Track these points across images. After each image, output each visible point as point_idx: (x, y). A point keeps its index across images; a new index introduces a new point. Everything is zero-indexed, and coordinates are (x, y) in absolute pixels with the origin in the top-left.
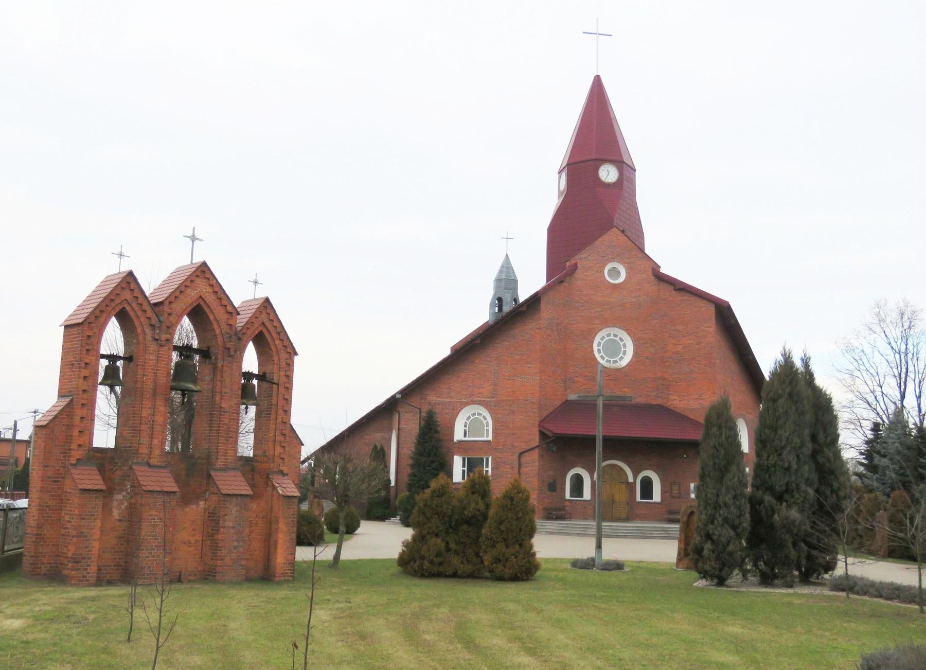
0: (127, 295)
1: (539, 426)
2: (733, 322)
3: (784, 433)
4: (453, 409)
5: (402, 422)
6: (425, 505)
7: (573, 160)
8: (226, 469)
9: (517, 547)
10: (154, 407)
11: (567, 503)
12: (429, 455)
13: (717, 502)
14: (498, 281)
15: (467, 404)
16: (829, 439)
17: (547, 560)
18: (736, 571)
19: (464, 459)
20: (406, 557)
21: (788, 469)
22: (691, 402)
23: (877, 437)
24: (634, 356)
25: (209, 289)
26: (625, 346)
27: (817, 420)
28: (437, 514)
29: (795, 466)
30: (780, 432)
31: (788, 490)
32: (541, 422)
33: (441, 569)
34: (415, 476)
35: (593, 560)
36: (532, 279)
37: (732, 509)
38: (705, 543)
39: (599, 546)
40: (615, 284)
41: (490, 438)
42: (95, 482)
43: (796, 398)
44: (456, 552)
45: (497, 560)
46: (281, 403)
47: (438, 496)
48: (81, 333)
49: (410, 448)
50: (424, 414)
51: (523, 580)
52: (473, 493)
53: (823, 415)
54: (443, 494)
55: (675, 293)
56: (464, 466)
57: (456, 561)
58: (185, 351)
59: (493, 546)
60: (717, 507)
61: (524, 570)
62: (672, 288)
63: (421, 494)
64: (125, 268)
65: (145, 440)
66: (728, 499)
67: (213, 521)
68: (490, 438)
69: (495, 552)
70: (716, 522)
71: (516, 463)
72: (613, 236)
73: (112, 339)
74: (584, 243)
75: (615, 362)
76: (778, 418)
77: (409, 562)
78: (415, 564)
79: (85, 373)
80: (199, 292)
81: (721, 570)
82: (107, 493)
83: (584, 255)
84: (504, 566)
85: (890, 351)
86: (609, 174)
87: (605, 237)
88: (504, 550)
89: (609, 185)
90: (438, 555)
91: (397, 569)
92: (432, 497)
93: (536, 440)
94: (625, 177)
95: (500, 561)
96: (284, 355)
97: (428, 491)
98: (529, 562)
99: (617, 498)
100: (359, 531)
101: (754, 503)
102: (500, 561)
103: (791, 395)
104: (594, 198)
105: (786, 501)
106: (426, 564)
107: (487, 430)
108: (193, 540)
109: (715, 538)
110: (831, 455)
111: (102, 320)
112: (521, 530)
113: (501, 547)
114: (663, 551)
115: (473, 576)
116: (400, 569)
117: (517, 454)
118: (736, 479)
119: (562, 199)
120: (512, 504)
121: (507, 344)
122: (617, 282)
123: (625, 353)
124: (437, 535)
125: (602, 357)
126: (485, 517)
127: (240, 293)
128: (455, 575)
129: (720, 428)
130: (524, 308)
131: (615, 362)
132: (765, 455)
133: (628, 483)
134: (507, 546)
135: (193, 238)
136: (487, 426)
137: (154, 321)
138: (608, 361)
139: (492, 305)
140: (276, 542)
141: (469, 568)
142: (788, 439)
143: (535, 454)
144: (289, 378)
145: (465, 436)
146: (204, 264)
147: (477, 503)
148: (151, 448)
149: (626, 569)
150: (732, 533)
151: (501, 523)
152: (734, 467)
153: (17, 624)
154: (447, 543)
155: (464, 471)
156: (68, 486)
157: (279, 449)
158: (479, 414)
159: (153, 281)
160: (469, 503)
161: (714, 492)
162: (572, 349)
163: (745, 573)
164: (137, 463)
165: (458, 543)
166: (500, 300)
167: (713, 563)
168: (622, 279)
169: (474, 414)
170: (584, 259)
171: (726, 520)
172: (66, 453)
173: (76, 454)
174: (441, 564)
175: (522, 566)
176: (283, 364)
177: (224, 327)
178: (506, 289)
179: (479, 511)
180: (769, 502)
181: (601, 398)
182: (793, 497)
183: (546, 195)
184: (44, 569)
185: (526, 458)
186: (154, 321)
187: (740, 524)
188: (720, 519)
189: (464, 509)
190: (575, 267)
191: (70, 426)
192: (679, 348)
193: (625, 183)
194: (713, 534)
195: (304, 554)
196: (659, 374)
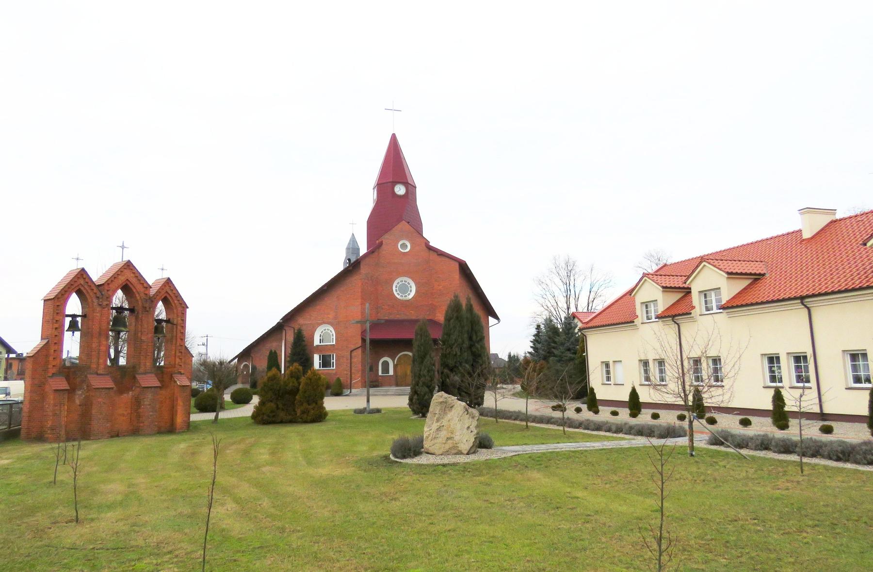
0: (82, 282)
3: (453, 337)
8: (145, 373)
10: (100, 342)
14: (348, 249)
15: (321, 324)
17: (332, 412)
21: (456, 355)
23: (538, 332)
25: (132, 275)
27: (472, 329)
29: (459, 353)
31: (455, 366)
36: (363, 250)
39: (368, 401)
42: (64, 385)
44: (283, 410)
45: (303, 412)
46: (179, 334)
48: (54, 304)
49: (289, 351)
57: (282, 415)
58: (120, 310)
59: (302, 404)
60: (420, 377)
61: (320, 416)
64: (80, 266)
65: (94, 360)
66: (425, 372)
67: (137, 402)
69: (302, 408)
72: (403, 225)
73: (74, 306)
74: (387, 230)
78: (262, 418)
79: (56, 326)
80: (127, 277)
82: (71, 391)
83: (386, 236)
85: (561, 284)
86: (400, 190)
89: (403, 196)
90: (272, 412)
91: (251, 421)
96: (180, 309)
103: (457, 318)
104: (394, 201)
108: (125, 413)
111: (66, 296)
113: (305, 405)
115: (292, 421)
126: (298, 390)
127: (152, 276)
129: (421, 336)
135: (123, 247)
137: (99, 294)
139: (345, 263)
140: (176, 411)
141: (289, 417)
144: (184, 321)
146: (129, 261)
148: (98, 364)
149: (383, 412)
150: (427, 389)
153: (6, 462)
156: (48, 388)
157: (178, 360)
159: (96, 274)
162: (378, 290)
164: (90, 374)
165: (284, 405)
166: (349, 260)
168: (408, 250)
170: (386, 239)
172: (46, 370)
173: (52, 370)
176: (180, 314)
177: (142, 295)
183: (365, 201)
184: (33, 435)
185: (354, 354)
186: (99, 294)
190: (381, 244)
191: (47, 356)
195: (197, 417)
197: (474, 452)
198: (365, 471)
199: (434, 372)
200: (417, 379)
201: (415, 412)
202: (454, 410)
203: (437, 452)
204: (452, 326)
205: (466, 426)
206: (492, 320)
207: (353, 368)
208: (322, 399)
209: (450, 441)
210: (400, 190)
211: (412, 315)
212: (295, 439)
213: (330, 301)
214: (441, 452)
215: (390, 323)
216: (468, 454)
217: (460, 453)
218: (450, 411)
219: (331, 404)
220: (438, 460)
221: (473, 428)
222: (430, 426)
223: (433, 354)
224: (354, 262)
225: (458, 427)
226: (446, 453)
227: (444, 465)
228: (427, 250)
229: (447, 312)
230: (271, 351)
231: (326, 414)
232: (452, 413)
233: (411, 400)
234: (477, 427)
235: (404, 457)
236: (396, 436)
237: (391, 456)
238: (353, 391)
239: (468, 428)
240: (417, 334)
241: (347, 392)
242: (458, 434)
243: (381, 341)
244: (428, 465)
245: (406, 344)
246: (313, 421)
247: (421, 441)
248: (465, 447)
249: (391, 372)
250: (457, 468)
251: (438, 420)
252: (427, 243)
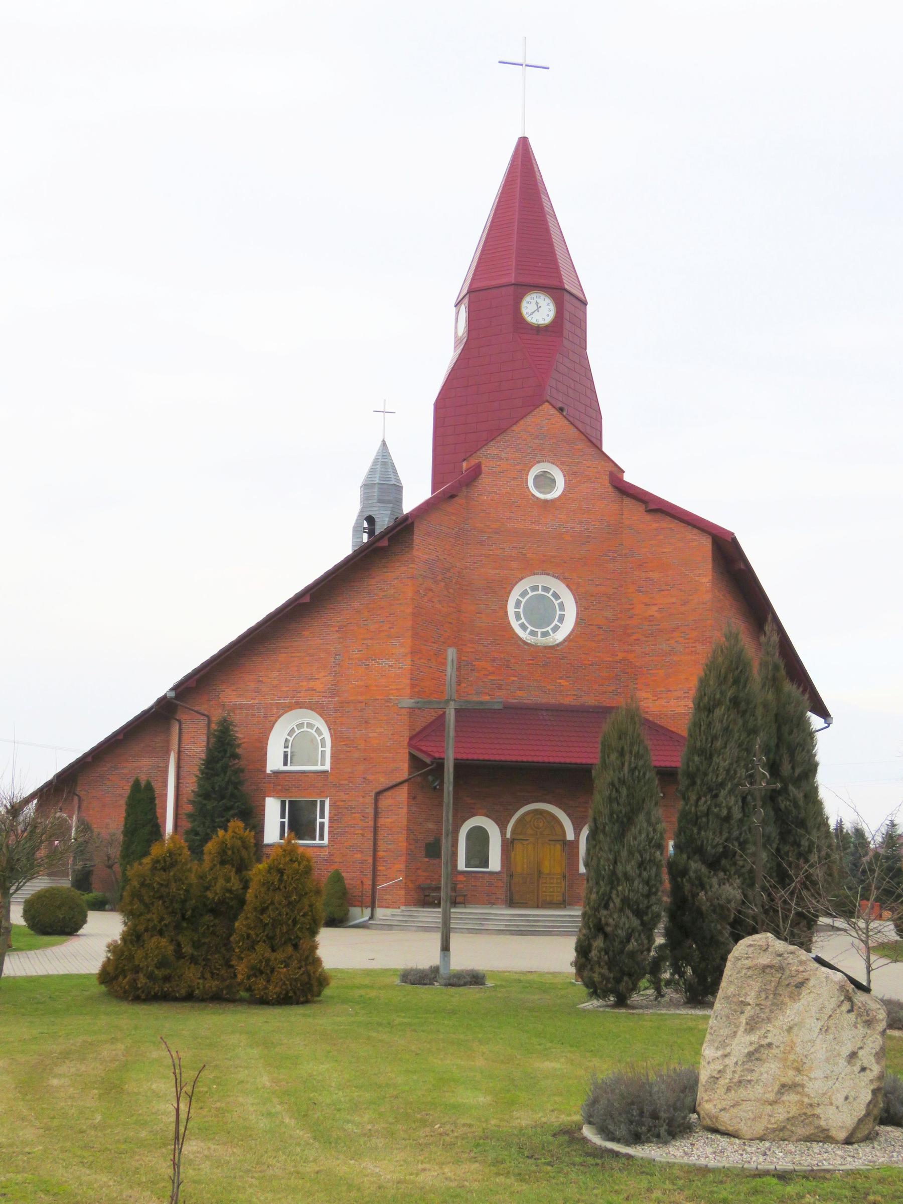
1: (410, 745)
2: (742, 567)
3: (722, 763)
4: (266, 716)
5: (185, 737)
6: (143, 884)
7: (477, 285)
9: (290, 949)
11: (461, 878)
12: (222, 797)
13: (614, 873)
14: (367, 486)
16: (798, 771)
18: (643, 983)
19: (283, 803)
20: (110, 969)
21: (728, 818)
22: (673, 702)
24: (577, 624)
26: (562, 606)
27: (780, 738)
28: (161, 897)
29: (737, 814)
30: (716, 759)
31: (727, 853)
32: (411, 739)
33: (167, 987)
34: (197, 834)
35: (435, 970)
36: (416, 490)
37: (636, 882)
38: (595, 937)
39: (445, 948)
40: (546, 501)
41: (327, 767)
43: (743, 706)
44: (193, 960)
45: (256, 971)
47: (164, 869)
49: (191, 786)
50: (214, 726)
51: (298, 1003)
52: (223, 863)
53: (791, 733)
54: (172, 865)
55: (648, 517)
56: (283, 816)
57: (191, 974)
59: (252, 948)
60: (613, 880)
61: (304, 987)
62: (641, 508)
63: (136, 865)
66: (631, 868)
68: (327, 767)
69: (253, 958)
70: (611, 905)
71: (370, 811)
72: (545, 418)
74: (495, 433)
75: (545, 634)
76: (715, 738)
77: (116, 978)
78: (130, 980)
81: (618, 981)
83: (492, 450)
84: (268, 981)
86: (538, 310)
87: (529, 419)
88: (267, 955)
89: (538, 329)
90: (162, 964)
92: (154, 869)
93: (403, 770)
94: (567, 315)
95: (261, 972)
97: (146, 860)
98: (307, 973)
99: (546, 869)
100: (85, 929)
101: (677, 872)
102: (261, 972)
103: (735, 702)
104: (519, 345)
105: (725, 871)
106: (142, 980)
107: (323, 752)
109: (608, 929)
110: (800, 796)
112: (295, 922)
113: (262, 949)
114: (552, 954)
115: (220, 998)
116: (103, 988)
117: (373, 794)
118: (643, 836)
119: (459, 351)
120: (281, 880)
121: (356, 604)
122: (549, 497)
123: (562, 618)
124: (161, 933)
125: (523, 627)
126: (242, 902)
128: (189, 997)
129: (622, 754)
130: (385, 543)
131: (545, 634)
132: (693, 797)
133: (565, 843)
134: (273, 950)
136: (323, 745)
138: (533, 633)
139: (357, 530)
141: (213, 985)
142: (728, 771)
143: (403, 793)
145: (285, 764)
147: (228, 880)
149: (489, 983)
150: (636, 922)
151: (263, 910)
152: (642, 817)
154: (179, 945)
155: (283, 824)
158: (310, 725)
160: (215, 879)
161: (611, 857)
162: (464, 616)
163: (657, 985)
165: (197, 945)
166: (371, 520)
167: (605, 971)
169: (300, 726)
170: (494, 457)
171: (626, 901)
174: (167, 979)
175: (296, 980)
178: (380, 501)
179: (230, 891)
180: (696, 871)
181: (452, 704)
182: (735, 864)
185: (386, 802)
187: (648, 907)
188: (617, 901)
189: (207, 889)
190: (476, 472)
192: (653, 611)
193: (567, 325)
194: (607, 924)
196: (621, 656)
197: (870, 1138)
198: (521, 1178)
199: (659, 866)
200: (604, 887)
201: (595, 990)
202: (806, 997)
203: (744, 1129)
204: (717, 727)
205: (846, 1051)
206: (816, 721)
207: (382, 846)
208: (314, 933)
209: (791, 1098)
210: (538, 310)
211: (565, 692)
212: (242, 1046)
213: (319, 637)
214: (759, 1128)
215: (517, 714)
216: (848, 1142)
217: (823, 1137)
218: (794, 997)
219: (335, 950)
220: (755, 1158)
221: (866, 1057)
222: (723, 1044)
223: (658, 812)
224: (389, 530)
225: (821, 1050)
226: (778, 1134)
227: (783, 1177)
228: (615, 495)
229: (704, 682)
230: (137, 783)
231: (323, 981)
232: (799, 1006)
233: (583, 950)
234: (880, 1055)
235: (637, 1139)
236: (605, 1069)
237: (588, 1132)
238: (380, 912)
239: (853, 1055)
240: (607, 747)
241: (360, 915)
242: (817, 1073)
243: (483, 764)
244: (726, 1173)
245: (567, 782)
246: (285, 1000)
247: (687, 1087)
248: (841, 1117)
249: (495, 863)
250: (828, 1186)
251: (751, 1027)
252: (615, 475)
